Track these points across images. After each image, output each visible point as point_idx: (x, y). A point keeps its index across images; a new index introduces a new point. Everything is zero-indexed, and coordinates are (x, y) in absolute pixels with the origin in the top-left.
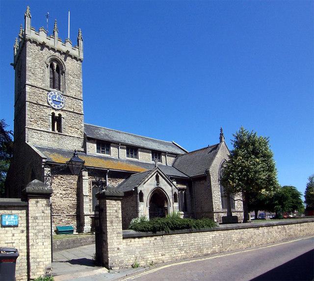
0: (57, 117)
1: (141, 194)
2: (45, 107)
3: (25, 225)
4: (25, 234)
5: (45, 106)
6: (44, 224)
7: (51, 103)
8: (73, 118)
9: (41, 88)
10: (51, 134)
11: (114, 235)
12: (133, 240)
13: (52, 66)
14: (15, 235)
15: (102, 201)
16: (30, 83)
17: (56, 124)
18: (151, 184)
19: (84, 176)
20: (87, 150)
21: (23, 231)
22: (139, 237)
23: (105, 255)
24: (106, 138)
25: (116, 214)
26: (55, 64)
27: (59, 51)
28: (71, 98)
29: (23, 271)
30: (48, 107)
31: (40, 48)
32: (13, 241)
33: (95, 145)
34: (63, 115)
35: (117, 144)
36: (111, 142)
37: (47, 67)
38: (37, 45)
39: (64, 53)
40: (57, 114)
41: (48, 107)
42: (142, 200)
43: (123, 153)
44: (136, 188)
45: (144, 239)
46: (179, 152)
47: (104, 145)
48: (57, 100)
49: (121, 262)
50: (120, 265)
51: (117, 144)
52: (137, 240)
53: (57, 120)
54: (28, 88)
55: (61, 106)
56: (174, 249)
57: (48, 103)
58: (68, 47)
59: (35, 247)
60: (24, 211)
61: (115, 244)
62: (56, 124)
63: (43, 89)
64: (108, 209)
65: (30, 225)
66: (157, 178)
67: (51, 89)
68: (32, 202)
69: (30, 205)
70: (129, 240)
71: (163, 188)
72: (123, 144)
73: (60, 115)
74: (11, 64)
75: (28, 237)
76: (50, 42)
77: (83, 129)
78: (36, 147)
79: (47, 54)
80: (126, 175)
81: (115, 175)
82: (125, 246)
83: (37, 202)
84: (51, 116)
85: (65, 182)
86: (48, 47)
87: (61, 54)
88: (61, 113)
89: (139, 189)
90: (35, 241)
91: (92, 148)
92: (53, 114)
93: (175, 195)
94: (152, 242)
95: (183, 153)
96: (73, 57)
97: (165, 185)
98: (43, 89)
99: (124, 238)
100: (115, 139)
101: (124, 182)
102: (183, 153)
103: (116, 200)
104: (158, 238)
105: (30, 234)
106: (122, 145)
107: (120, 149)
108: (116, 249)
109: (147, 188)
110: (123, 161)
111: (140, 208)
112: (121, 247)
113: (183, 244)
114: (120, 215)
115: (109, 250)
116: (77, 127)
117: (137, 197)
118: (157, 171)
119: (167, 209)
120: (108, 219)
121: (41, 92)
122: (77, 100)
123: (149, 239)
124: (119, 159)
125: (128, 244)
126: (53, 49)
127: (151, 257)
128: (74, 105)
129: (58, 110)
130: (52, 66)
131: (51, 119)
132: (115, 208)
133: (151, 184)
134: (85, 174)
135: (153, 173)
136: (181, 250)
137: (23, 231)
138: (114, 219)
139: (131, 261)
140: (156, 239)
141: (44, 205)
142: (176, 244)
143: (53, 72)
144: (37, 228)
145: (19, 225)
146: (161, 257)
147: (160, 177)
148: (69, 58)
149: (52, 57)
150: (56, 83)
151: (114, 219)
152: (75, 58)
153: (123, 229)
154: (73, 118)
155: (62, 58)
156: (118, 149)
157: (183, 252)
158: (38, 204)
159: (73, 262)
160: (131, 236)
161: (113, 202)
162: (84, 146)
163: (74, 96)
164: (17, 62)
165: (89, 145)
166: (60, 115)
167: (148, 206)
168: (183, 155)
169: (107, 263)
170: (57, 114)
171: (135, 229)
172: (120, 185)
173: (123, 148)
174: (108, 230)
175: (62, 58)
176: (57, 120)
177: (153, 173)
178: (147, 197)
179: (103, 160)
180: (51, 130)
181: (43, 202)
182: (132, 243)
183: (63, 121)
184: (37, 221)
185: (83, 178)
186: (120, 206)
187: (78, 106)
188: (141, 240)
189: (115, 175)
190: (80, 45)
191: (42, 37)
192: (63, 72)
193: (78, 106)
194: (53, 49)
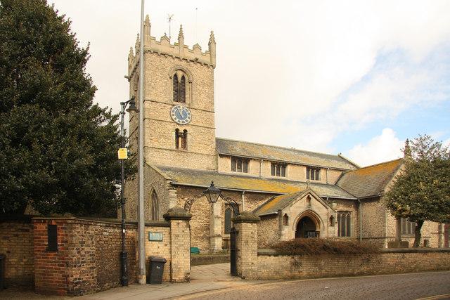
3: (169, 240)
4: (168, 247)
7: (175, 119)
12: (268, 258)
16: (150, 99)
17: (180, 139)
18: (300, 207)
29: (148, 126)
34: (190, 130)
40: (181, 130)
42: (286, 224)
44: (280, 211)
46: (347, 167)
53: (181, 136)
55: (187, 121)
57: (172, 119)
60: (169, 228)
66: (309, 198)
67: (175, 103)
68: (174, 223)
73: (185, 131)
74: (125, 77)
78: (159, 168)
81: (254, 195)
89: (284, 212)
91: (225, 166)
93: (332, 218)
95: (352, 169)
102: (352, 168)
109: (295, 211)
112: (255, 262)
118: (310, 193)
119: (319, 234)
161: (249, 225)
164: (132, 74)
166: (185, 131)
168: (351, 171)
169: (241, 274)
170: (181, 130)
171: (272, 248)
176: (181, 136)
177: (303, 196)
178: (293, 221)
180: (174, 148)
183: (189, 137)
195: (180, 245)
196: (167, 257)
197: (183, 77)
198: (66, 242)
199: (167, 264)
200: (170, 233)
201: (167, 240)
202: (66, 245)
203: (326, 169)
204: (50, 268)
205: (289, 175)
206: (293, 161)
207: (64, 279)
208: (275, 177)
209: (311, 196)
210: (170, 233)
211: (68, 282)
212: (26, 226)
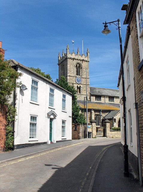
1: (115, 120)
9: (73, 76)
13: (77, 66)
24: (99, 94)
26: (78, 65)
33: (95, 97)
35: (104, 96)
38: (71, 59)
39: (82, 60)
40: (79, 86)
42: (115, 122)
43: (107, 100)
44: (113, 117)
47: (98, 97)
51: (104, 96)
54: (68, 77)
58: (83, 58)
67: (77, 76)
73: (80, 86)
76: (76, 57)
79: (75, 62)
80: (109, 111)
81: (104, 111)
89: (114, 118)
91: (93, 99)
92: (78, 86)
100: (103, 94)
101: (108, 114)
104: (119, 132)
110: (107, 104)
111: (114, 125)
124: (105, 103)
126: (78, 60)
127: (116, 136)
129: (79, 84)
130: (77, 66)
134: (93, 111)
148: (84, 62)
150: (78, 73)
152: (86, 61)
155: (81, 62)
159: (52, 165)
165: (92, 97)
166: (80, 86)
170: (79, 86)
172: (106, 116)
175: (81, 62)
179: (96, 104)
189: (104, 111)
191: (73, 56)
192: (81, 68)
194: (78, 60)
197: (79, 66)
201: (91, 127)
206: (116, 96)
208: (110, 102)
211: (79, 136)
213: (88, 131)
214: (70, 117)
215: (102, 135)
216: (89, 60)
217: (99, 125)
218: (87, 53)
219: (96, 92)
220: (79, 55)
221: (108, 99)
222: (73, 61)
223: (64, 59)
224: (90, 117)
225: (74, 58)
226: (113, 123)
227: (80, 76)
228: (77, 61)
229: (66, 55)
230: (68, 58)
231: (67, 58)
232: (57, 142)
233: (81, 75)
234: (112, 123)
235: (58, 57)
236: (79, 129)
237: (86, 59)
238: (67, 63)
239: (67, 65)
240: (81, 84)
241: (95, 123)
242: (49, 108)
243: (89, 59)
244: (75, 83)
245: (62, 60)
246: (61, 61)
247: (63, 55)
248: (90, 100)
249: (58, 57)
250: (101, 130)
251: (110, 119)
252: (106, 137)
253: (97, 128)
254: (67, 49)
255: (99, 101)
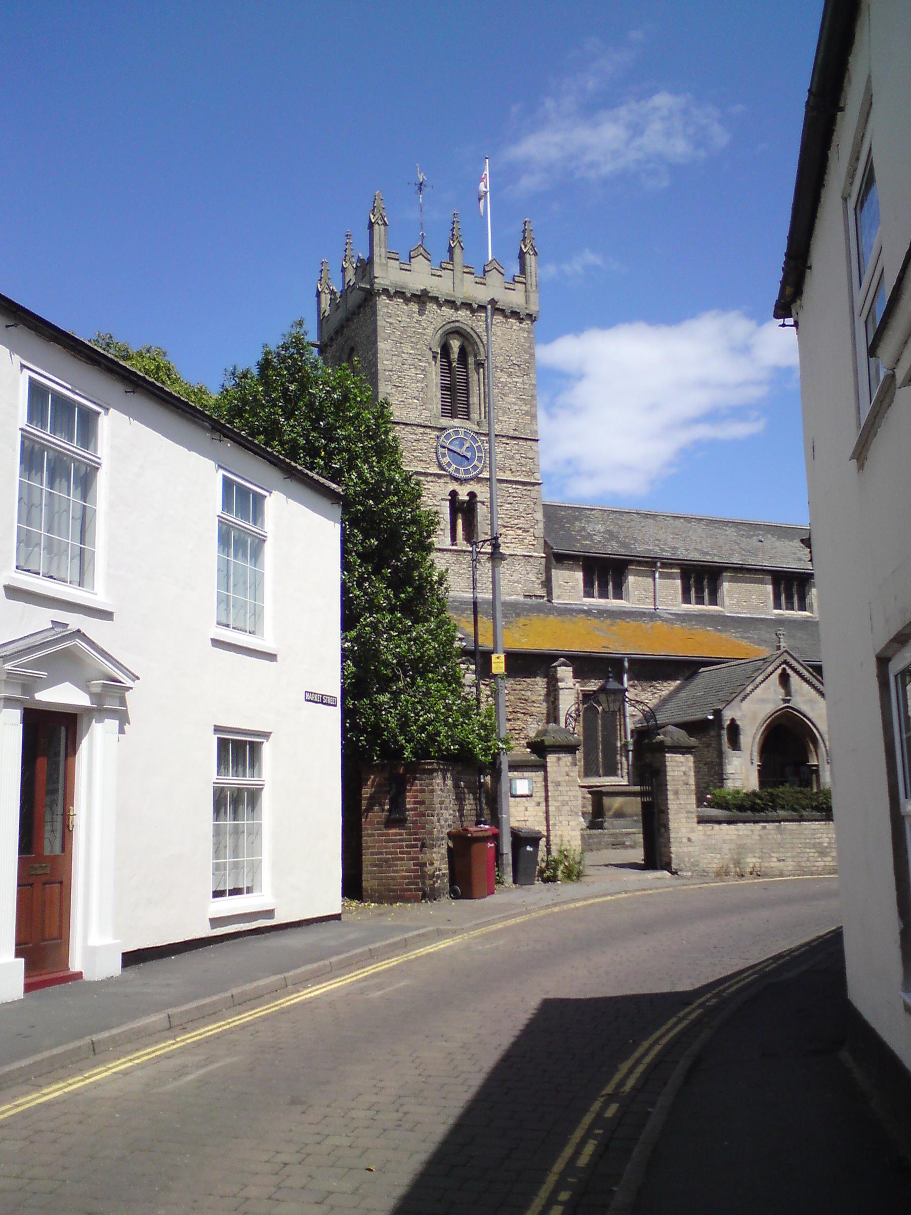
0: (463, 502)
1: (734, 730)
2: (429, 479)
3: (543, 794)
4: (543, 807)
5: (431, 474)
6: (570, 793)
7: (449, 465)
8: (510, 499)
10: (448, 555)
11: (681, 815)
12: (716, 827)
14: (529, 808)
15: (658, 755)
17: (460, 522)
18: (763, 701)
19: (562, 680)
20: (556, 592)
21: (538, 804)
22: (729, 822)
23: (664, 850)
24: (613, 549)
25: (684, 778)
26: (455, 344)
27: (467, 305)
28: (505, 440)
30: (439, 476)
31: (415, 307)
32: (526, 819)
33: (579, 575)
34: (482, 492)
36: (631, 562)
37: (435, 357)
38: (407, 300)
40: (463, 496)
41: (439, 476)
42: (735, 744)
44: (718, 713)
45: (740, 826)
48: (463, 451)
49: (693, 865)
50: (693, 869)
52: (724, 826)
56: (808, 850)
59: (557, 828)
60: (541, 774)
61: (683, 830)
62: (460, 522)
63: (424, 427)
64: (669, 769)
65: (550, 794)
66: (784, 679)
67: (445, 422)
68: (551, 759)
69: (548, 764)
70: (709, 826)
71: (804, 708)
72: (667, 564)
73: (472, 495)
75: (547, 812)
76: (441, 286)
77: (539, 530)
82: (702, 837)
83: (559, 759)
84: (448, 503)
85: (512, 698)
86: (435, 299)
87: (473, 311)
88: (473, 487)
90: (557, 819)
92: (454, 494)
94: (757, 833)
96: (508, 312)
97: (811, 701)
98: (424, 427)
99: (699, 822)
100: (640, 549)
101: (678, 690)
103: (683, 753)
105: (551, 808)
106: (664, 565)
107: (657, 580)
108: (685, 840)
112: (694, 837)
113: (829, 843)
114: (692, 781)
115: (672, 840)
116: (521, 522)
117: (719, 736)
118: (785, 662)
119: (817, 772)
120: (669, 787)
121: (419, 437)
122: (521, 442)
123: (750, 826)
125: (709, 833)
126: (451, 303)
128: (512, 458)
129: (466, 481)
130: (445, 349)
131: (447, 510)
132: (683, 769)
133: (763, 701)
134: (565, 673)
135: (770, 669)
136: (823, 853)
137: (538, 804)
138: (682, 788)
139: (715, 866)
140: (764, 828)
141: (568, 764)
142: (813, 841)
143: (448, 369)
144: (560, 798)
145: (534, 795)
146: (778, 864)
147: (794, 679)
149: (448, 327)
151: (682, 788)
152: (515, 314)
153: (698, 807)
154: (510, 499)
156: (654, 579)
157: (829, 859)
158: (560, 762)
160: (714, 819)
161: (679, 758)
162: (547, 584)
163: (511, 433)
164: (332, 339)
165: (560, 576)
166: (472, 495)
167: (757, 762)
170: (463, 496)
172: (665, 701)
173: (669, 576)
174: (669, 806)
177: (770, 669)
181: (566, 759)
182: (713, 832)
184: (560, 788)
185: (560, 685)
186: (691, 764)
187: (523, 461)
188: (732, 827)
190: (528, 269)
192: (479, 365)
193: (523, 461)
194: (451, 303)
195: (564, 803)
196: (543, 829)
197: (463, 351)
198: (422, 803)
199: (542, 842)
200: (546, 779)
201: (540, 794)
202: (422, 808)
203: (811, 552)
204: (391, 853)
205: (727, 601)
206: (736, 560)
207: (417, 871)
208: (693, 608)
209: (789, 671)
210: (546, 779)
211: (423, 876)
212: (582, 774)
213: (514, 824)
214: (322, 700)
215: (638, 855)
216: (533, 308)
217: (611, 771)
218: (522, 256)
219: (590, 536)
220: (459, 268)
221: (678, 582)
222: (421, 312)
223: (354, 298)
224: (475, 640)
225: (425, 292)
226: (720, 754)
227: (468, 424)
228: (447, 311)
229: (365, 267)
230: (378, 294)
231: (369, 297)
232: (131, 959)
233: (475, 416)
234: (711, 755)
235: (318, 294)
236: (425, 808)
237: (514, 298)
238: (375, 331)
239: (376, 342)
240: (479, 480)
241: (567, 758)
242: (216, 643)
243: (534, 297)
244: (435, 470)
245: (340, 314)
246: (334, 324)
247: (350, 275)
248: (550, 593)
249: (318, 294)
250: (628, 810)
251: (694, 727)
252: (667, 866)
253: (598, 796)
254: (371, 225)
255: (612, 603)
